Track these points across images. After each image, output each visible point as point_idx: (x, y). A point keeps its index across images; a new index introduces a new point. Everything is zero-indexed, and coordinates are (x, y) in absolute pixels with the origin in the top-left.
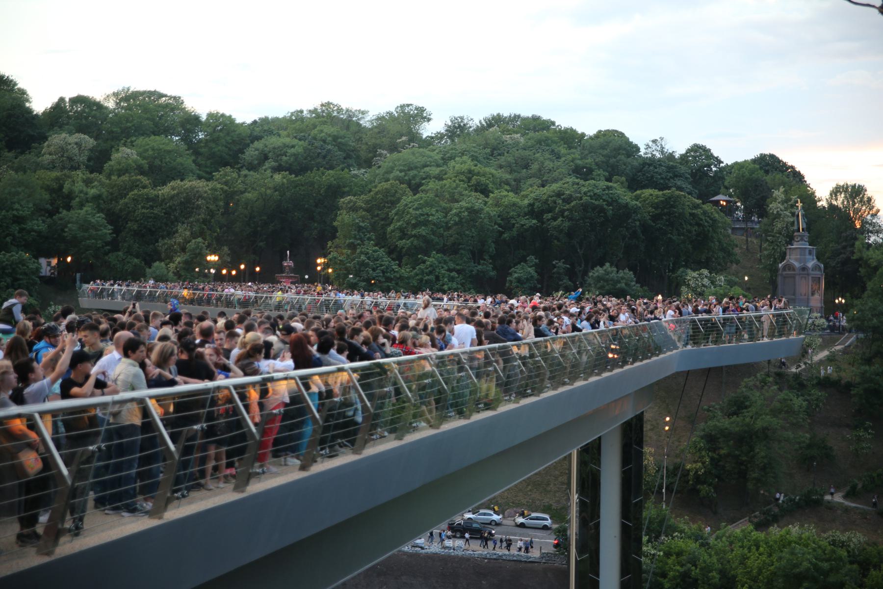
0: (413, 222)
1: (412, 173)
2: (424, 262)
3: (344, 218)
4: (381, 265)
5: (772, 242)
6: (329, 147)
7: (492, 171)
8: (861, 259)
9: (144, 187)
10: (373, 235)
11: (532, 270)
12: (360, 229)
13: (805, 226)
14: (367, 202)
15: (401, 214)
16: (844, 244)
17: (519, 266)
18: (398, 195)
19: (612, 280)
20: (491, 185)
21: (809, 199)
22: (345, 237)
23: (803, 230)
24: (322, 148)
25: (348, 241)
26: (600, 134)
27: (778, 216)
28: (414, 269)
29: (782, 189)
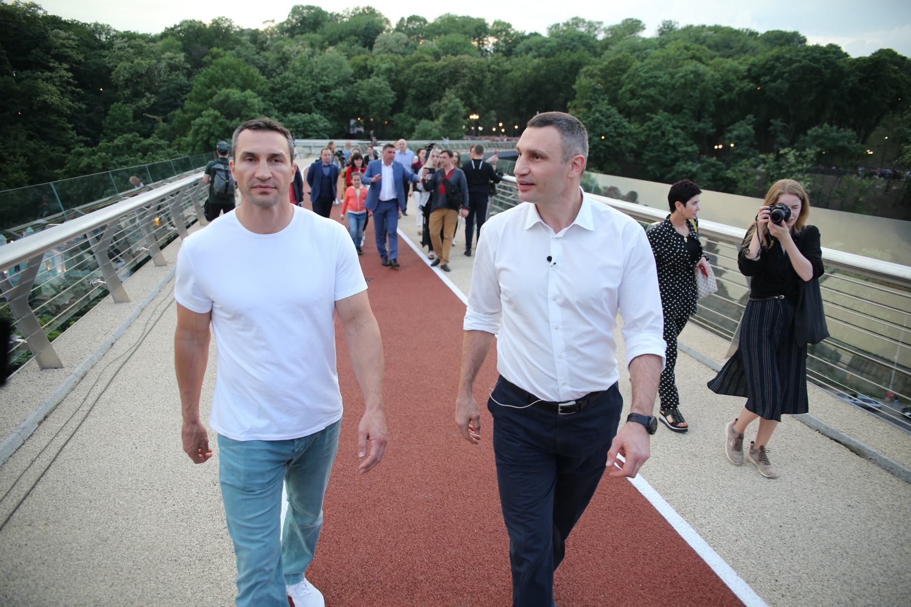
0: (643, 83)
2: (651, 119)
3: (582, 81)
6: (575, 43)
9: (427, 61)
10: (607, 97)
11: (750, 128)
12: (595, 90)
14: (601, 70)
15: (632, 77)
17: (738, 124)
18: (628, 64)
22: (582, 98)
24: (570, 44)
28: (642, 125)
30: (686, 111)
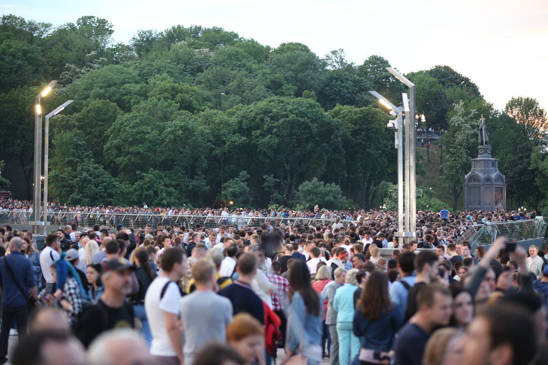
0: (130, 139)
1: (113, 89)
2: (142, 178)
4: (103, 182)
5: (453, 154)
6: (19, 62)
7: (192, 88)
8: (537, 169)
11: (244, 185)
12: (77, 146)
13: (488, 140)
14: (79, 120)
16: (520, 155)
19: (320, 193)
20: (195, 102)
21: (486, 110)
23: (486, 142)
25: (67, 159)
26: (285, 48)
27: (459, 128)
28: (133, 184)
29: (462, 103)
30: (177, 167)
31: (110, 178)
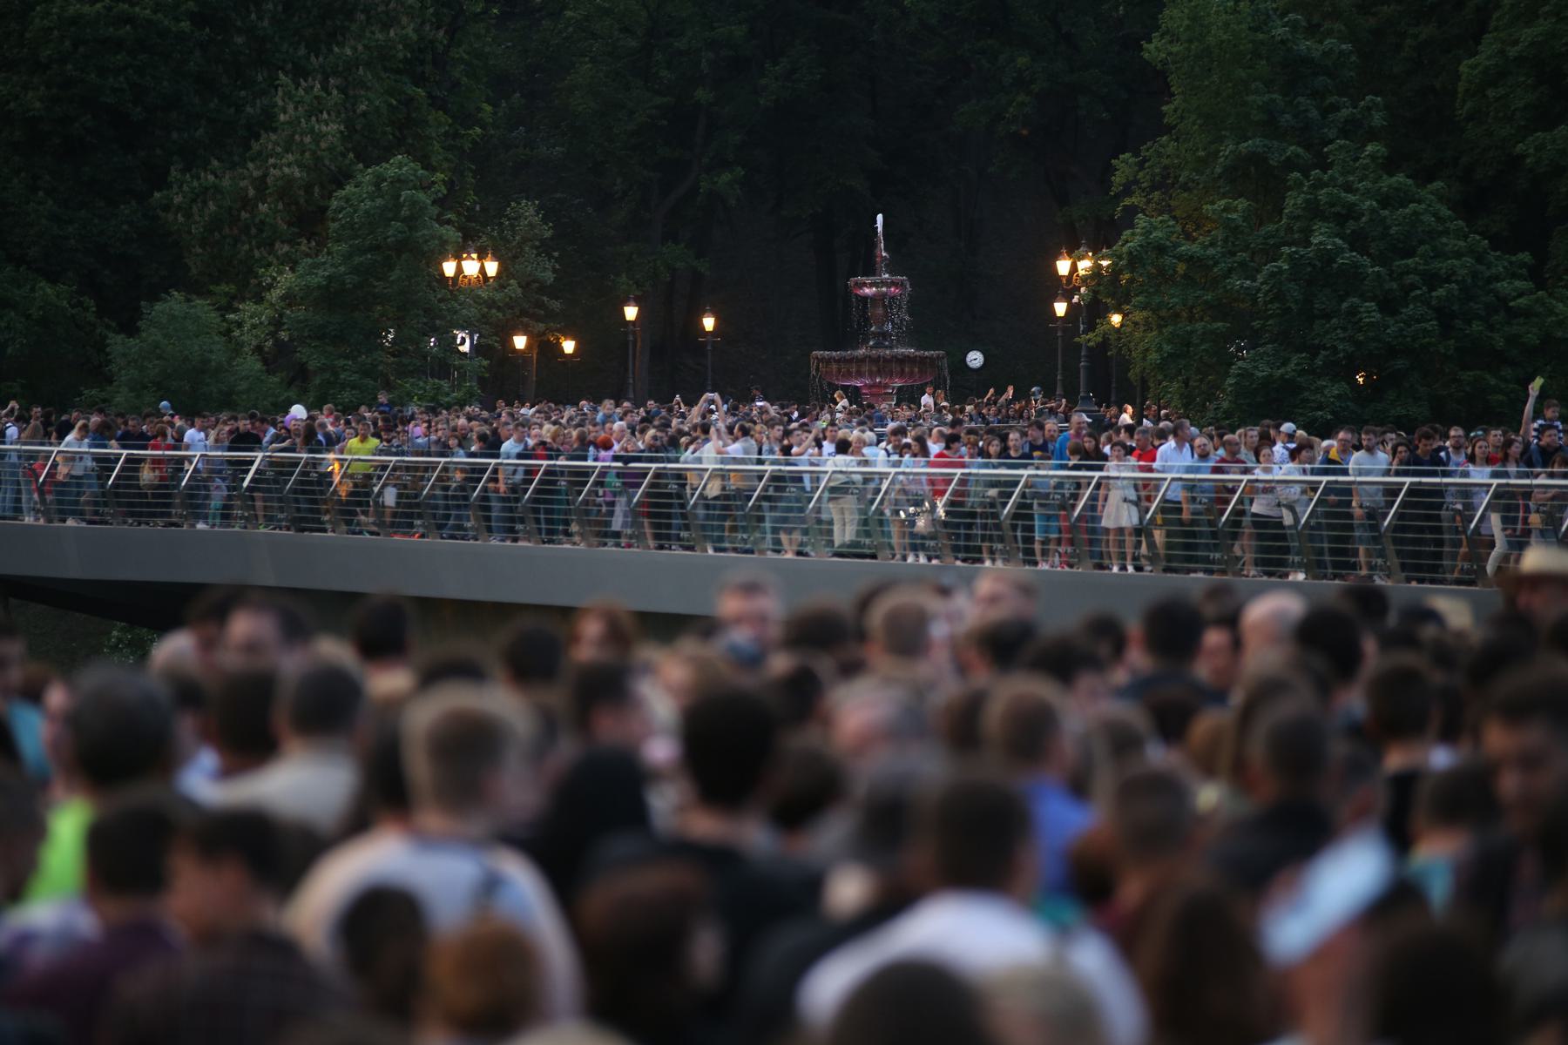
4: (1432, 280)
25: (1227, 148)
31: (1480, 259)
